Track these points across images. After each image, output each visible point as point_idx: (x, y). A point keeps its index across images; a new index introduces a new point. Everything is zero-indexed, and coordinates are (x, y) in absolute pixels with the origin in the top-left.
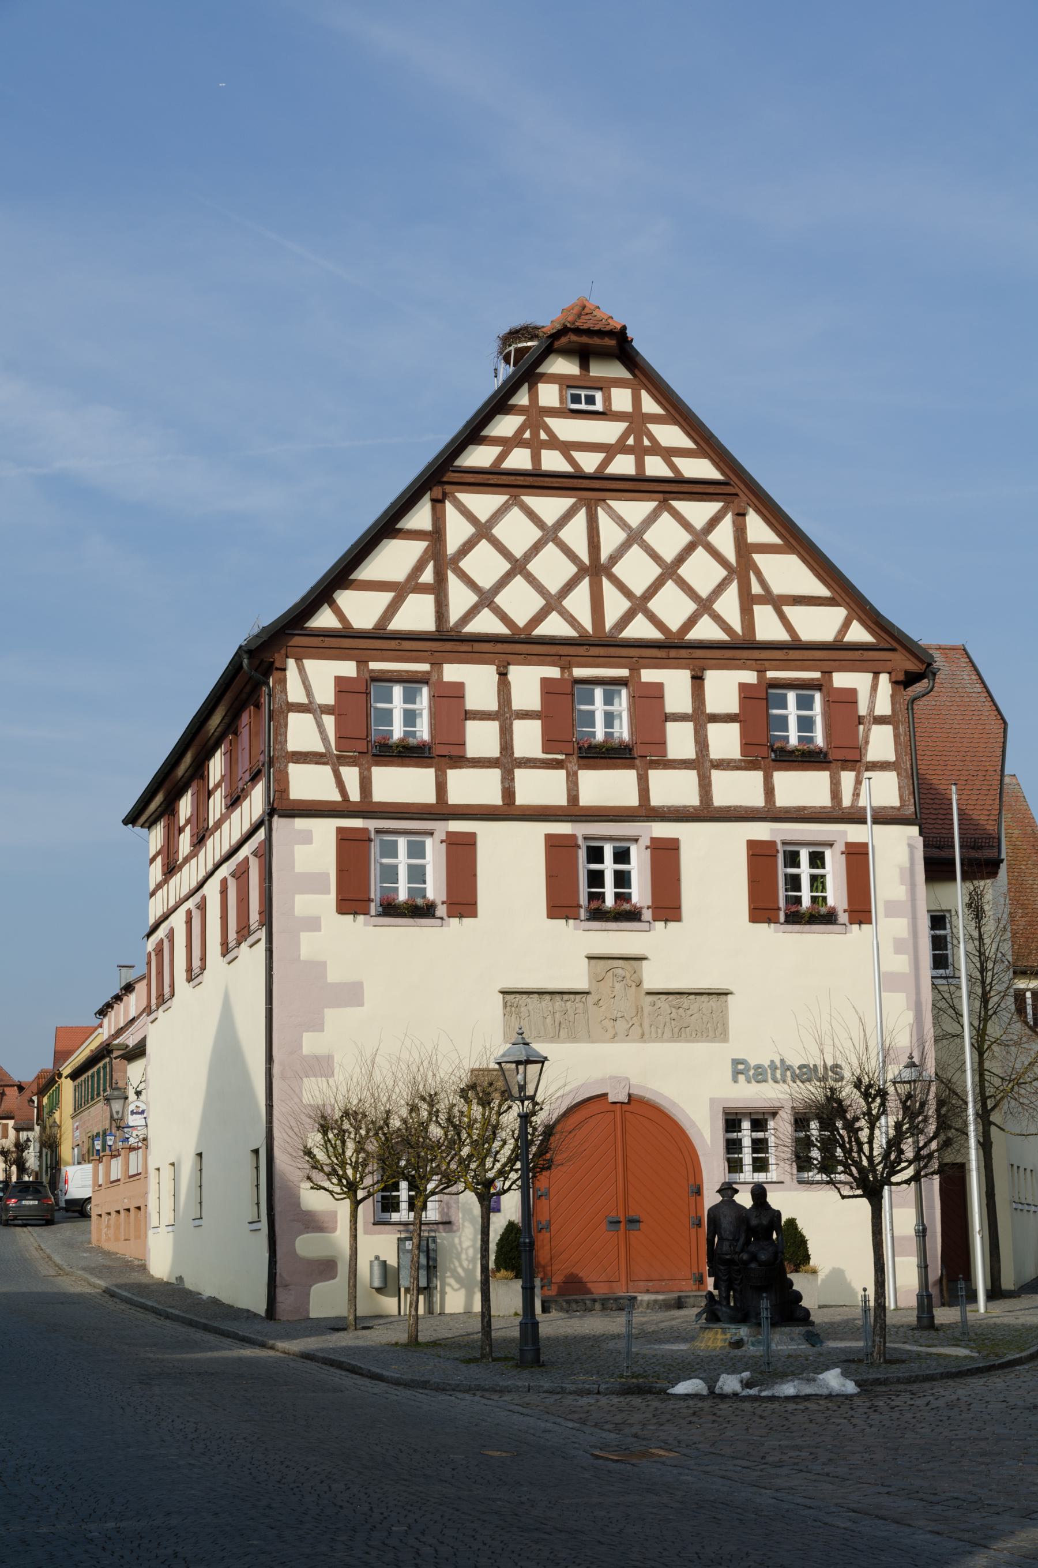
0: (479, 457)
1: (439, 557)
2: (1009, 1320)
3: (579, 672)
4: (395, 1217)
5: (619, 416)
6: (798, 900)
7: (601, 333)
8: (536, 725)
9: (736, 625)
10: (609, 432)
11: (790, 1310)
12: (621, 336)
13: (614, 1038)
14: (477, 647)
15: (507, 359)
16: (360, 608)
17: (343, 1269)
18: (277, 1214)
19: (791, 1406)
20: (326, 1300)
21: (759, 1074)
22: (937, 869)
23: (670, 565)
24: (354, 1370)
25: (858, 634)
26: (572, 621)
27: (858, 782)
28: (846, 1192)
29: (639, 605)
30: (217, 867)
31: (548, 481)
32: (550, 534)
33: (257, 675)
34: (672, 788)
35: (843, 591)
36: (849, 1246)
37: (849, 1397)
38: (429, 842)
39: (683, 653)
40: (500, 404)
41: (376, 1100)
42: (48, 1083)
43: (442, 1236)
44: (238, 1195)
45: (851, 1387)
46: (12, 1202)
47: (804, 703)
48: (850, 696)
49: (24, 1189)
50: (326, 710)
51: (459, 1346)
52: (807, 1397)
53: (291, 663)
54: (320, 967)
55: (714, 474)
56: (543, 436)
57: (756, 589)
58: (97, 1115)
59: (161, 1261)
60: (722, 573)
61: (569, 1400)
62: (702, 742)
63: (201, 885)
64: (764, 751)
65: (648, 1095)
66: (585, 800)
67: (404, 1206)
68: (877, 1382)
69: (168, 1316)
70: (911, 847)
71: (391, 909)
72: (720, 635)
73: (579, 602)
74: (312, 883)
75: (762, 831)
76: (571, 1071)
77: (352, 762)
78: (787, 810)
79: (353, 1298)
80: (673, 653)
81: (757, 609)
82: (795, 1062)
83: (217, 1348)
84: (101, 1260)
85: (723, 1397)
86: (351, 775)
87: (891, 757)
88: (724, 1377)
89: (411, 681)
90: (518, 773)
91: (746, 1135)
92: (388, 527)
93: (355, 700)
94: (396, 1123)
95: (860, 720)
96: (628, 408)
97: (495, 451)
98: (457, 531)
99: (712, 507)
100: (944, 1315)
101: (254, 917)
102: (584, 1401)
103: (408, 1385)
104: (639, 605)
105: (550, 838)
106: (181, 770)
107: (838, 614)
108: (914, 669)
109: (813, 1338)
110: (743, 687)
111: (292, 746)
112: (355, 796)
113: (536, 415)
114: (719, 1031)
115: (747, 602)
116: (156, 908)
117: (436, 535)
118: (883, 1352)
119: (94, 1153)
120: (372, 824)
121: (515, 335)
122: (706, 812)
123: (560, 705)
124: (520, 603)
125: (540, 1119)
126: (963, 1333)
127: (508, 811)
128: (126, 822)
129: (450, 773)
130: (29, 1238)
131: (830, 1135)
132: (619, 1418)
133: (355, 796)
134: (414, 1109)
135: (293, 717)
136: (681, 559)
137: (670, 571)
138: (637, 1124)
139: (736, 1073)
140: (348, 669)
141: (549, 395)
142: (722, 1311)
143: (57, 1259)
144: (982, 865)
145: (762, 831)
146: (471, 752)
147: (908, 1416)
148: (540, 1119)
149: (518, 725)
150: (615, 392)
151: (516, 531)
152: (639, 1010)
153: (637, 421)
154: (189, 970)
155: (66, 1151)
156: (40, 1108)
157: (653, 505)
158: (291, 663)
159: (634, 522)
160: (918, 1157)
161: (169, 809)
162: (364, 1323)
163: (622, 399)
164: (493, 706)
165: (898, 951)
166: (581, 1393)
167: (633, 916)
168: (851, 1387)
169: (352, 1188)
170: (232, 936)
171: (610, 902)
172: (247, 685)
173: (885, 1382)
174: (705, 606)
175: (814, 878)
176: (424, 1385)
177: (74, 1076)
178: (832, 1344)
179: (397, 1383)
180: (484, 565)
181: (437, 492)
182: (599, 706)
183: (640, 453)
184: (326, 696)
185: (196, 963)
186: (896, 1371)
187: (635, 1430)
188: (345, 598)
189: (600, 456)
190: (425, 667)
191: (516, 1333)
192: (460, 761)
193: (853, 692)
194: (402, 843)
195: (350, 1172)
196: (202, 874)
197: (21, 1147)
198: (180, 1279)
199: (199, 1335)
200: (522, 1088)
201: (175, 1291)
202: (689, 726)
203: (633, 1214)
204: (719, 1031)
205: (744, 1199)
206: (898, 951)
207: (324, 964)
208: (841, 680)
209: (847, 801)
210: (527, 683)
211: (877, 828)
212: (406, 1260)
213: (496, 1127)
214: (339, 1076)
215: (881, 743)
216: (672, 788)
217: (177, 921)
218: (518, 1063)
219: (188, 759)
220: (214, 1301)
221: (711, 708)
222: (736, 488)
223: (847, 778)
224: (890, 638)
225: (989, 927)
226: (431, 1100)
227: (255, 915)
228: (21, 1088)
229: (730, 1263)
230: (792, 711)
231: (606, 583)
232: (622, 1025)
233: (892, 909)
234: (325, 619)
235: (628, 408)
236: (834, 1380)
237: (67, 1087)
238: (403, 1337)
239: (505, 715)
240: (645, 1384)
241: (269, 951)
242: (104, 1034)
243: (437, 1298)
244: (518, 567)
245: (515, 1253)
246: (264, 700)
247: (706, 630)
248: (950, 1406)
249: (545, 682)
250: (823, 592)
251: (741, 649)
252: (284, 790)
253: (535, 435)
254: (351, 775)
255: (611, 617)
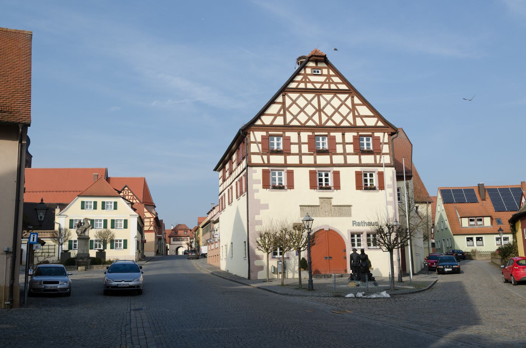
0: (293, 85)
1: (284, 108)
2: (418, 280)
3: (316, 134)
4: (276, 256)
5: (325, 75)
6: (367, 185)
7: (320, 56)
8: (307, 146)
9: (352, 122)
10: (322, 79)
11: (371, 278)
12: (325, 57)
13: (325, 216)
14: (293, 128)
15: (298, 64)
16: (266, 120)
17: (265, 268)
18: (250, 256)
19: (376, 300)
20: (261, 275)
21: (359, 224)
22: (399, 178)
23: (337, 109)
24: (270, 291)
25: (380, 124)
26: (314, 122)
27: (381, 158)
28: (384, 250)
29: (330, 118)
30: (235, 179)
31: (308, 90)
32: (309, 102)
33: (244, 135)
34: (338, 159)
35: (377, 114)
36: (381, 263)
37: (388, 298)
38: (283, 172)
39: (340, 129)
40: (297, 73)
41: (273, 230)
42: (197, 229)
43: (287, 261)
44: (241, 252)
45: (388, 296)
46: (190, 254)
47: (368, 140)
48: (378, 138)
49: (192, 251)
50: (259, 143)
51: (293, 286)
52: (379, 298)
53: (251, 132)
54: (259, 201)
55: (347, 88)
56: (307, 80)
57: (356, 114)
58: (208, 235)
59: (223, 266)
60: (349, 110)
61: (322, 298)
62: (344, 149)
63: (231, 183)
64: (359, 151)
65: (333, 229)
66: (318, 162)
67: (278, 254)
68: (394, 294)
69: (226, 279)
70: (393, 172)
71: (274, 187)
72: (348, 125)
73: (316, 118)
74: (257, 182)
75: (359, 169)
76: (319, 223)
77: (265, 155)
78: (364, 164)
79: (268, 275)
80: (338, 129)
81: (357, 118)
82: (367, 221)
83: (233, 285)
84: (210, 266)
85: (358, 298)
86: (265, 157)
87: (388, 152)
88: (358, 293)
89: (278, 136)
90: (303, 156)
91: (356, 238)
92: (272, 101)
93: (266, 140)
94: (277, 235)
95: (381, 144)
96: (327, 73)
97: (297, 84)
98: (288, 102)
99: (347, 95)
100: (404, 279)
101: (244, 190)
102: (326, 298)
103: (283, 294)
104: (330, 118)
105: (310, 171)
106: (226, 158)
107: (376, 119)
108: (394, 132)
109: (376, 284)
110: (354, 136)
111: (252, 151)
112: (266, 162)
113: (306, 76)
114: (349, 214)
115: (354, 117)
116: (221, 189)
117: (284, 103)
118: (394, 288)
119: (207, 243)
120: (270, 168)
121: (300, 58)
122: (346, 165)
123: (312, 141)
124: (303, 118)
125: (311, 234)
126: (410, 283)
127: (301, 165)
128: (214, 170)
129: (288, 157)
130: (194, 262)
131: (377, 237)
132: (335, 303)
133: (266, 162)
134: (282, 232)
135: (252, 144)
136: (339, 107)
137: (337, 110)
138: (332, 235)
139: (353, 224)
140: (264, 134)
141: (308, 71)
142: (354, 278)
143: (200, 266)
144: (409, 177)
145: (359, 169)
146: (292, 152)
147: (405, 303)
148: (311, 234)
149: (303, 146)
150: (323, 70)
151: (302, 102)
152: (331, 210)
153: (329, 76)
154: (229, 202)
155: (201, 243)
156: (195, 234)
157: (332, 95)
158: (251, 132)
159: (328, 99)
160: (401, 242)
161: (224, 167)
162: (270, 280)
163: (325, 71)
164: (297, 141)
165: (390, 196)
166: (324, 297)
167: (329, 188)
168: (388, 296)
169: (267, 250)
170: (239, 194)
171: (324, 185)
172: (241, 138)
173: (396, 295)
174: (345, 118)
175: (371, 180)
176: (287, 294)
177: (202, 227)
178: (380, 286)
179: (281, 294)
180: (294, 110)
181: (284, 93)
182: (321, 141)
183: (329, 83)
184: (259, 139)
185: (230, 201)
186: (397, 292)
187: (340, 305)
188: (263, 118)
189: (320, 85)
190: (281, 133)
191: (308, 282)
192: (290, 154)
193: (379, 137)
194: (277, 172)
195: (267, 246)
196: (231, 181)
197: (191, 243)
198: (228, 270)
199: (233, 283)
200: (308, 226)
201: (227, 273)
202: (342, 145)
203: (330, 256)
204: (349, 214)
205: (359, 252)
206: (390, 196)
207: (260, 200)
208: (376, 134)
209: (378, 162)
210: (305, 136)
211: (386, 168)
212: (279, 266)
213: (302, 236)
214: (264, 225)
215: (386, 149)
216: (338, 159)
217: (226, 192)
218: (307, 221)
219: (228, 156)
220: (236, 275)
221: (346, 141)
222: (352, 91)
223: (378, 157)
224: (388, 125)
225: (410, 191)
226: (286, 230)
227: (244, 189)
228: (191, 230)
229: (355, 267)
230: (365, 142)
231: (322, 113)
232: (327, 213)
233: (389, 187)
234: (259, 122)
235: (327, 73)
236: (384, 294)
237: (201, 230)
238: (280, 284)
239: (300, 143)
240: (339, 295)
241: (248, 197)
242: (208, 218)
243: (286, 275)
244: (302, 110)
245: (303, 265)
246: (245, 141)
247: (345, 124)
248: (414, 300)
249: (309, 136)
250: (372, 114)
251: (353, 128)
252: (250, 161)
253: (306, 80)
254: (265, 157)
255: (323, 121)
